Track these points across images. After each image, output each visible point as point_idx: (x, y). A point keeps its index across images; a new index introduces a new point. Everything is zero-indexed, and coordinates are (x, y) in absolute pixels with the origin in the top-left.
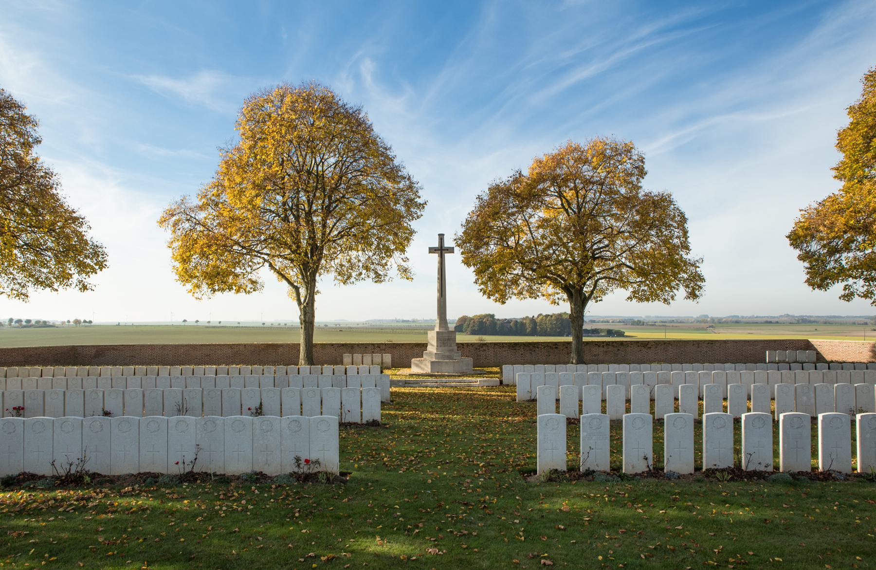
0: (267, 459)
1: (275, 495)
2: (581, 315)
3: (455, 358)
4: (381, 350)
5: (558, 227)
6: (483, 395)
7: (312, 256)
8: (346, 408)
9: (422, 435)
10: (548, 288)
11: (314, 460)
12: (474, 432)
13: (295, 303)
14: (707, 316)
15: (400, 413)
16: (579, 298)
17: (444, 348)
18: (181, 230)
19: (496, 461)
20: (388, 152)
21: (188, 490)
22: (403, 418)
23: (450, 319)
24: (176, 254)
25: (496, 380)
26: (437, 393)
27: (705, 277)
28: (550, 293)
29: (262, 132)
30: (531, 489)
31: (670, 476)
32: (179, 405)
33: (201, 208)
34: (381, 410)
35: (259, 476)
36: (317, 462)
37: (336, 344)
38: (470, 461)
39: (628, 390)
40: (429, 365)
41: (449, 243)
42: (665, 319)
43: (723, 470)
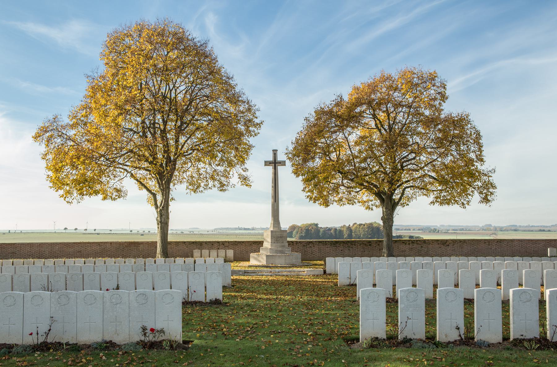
0: (116, 329)
1: (121, 361)
2: (391, 217)
3: (286, 253)
4: (225, 247)
5: (373, 143)
6: (309, 281)
7: (166, 166)
8: (192, 289)
9: (258, 311)
10: (365, 195)
11: (159, 329)
12: (303, 309)
13: (153, 208)
14: (490, 225)
15: (239, 294)
16: (390, 203)
17: (277, 244)
18: (54, 144)
19: (322, 331)
20: (231, 81)
21: (38, 358)
22: (242, 298)
23: (284, 227)
24: (49, 165)
25: (320, 270)
26: (271, 280)
27: (496, 185)
28: (364, 200)
29: (123, 62)
30: (355, 354)
31: (481, 345)
32: (44, 287)
33: (73, 126)
34: (223, 292)
35: (108, 345)
36: (162, 331)
37: (187, 242)
38: (299, 331)
39: (435, 274)
40: (265, 258)
41: (281, 157)
42: (456, 228)
43: (530, 340)
